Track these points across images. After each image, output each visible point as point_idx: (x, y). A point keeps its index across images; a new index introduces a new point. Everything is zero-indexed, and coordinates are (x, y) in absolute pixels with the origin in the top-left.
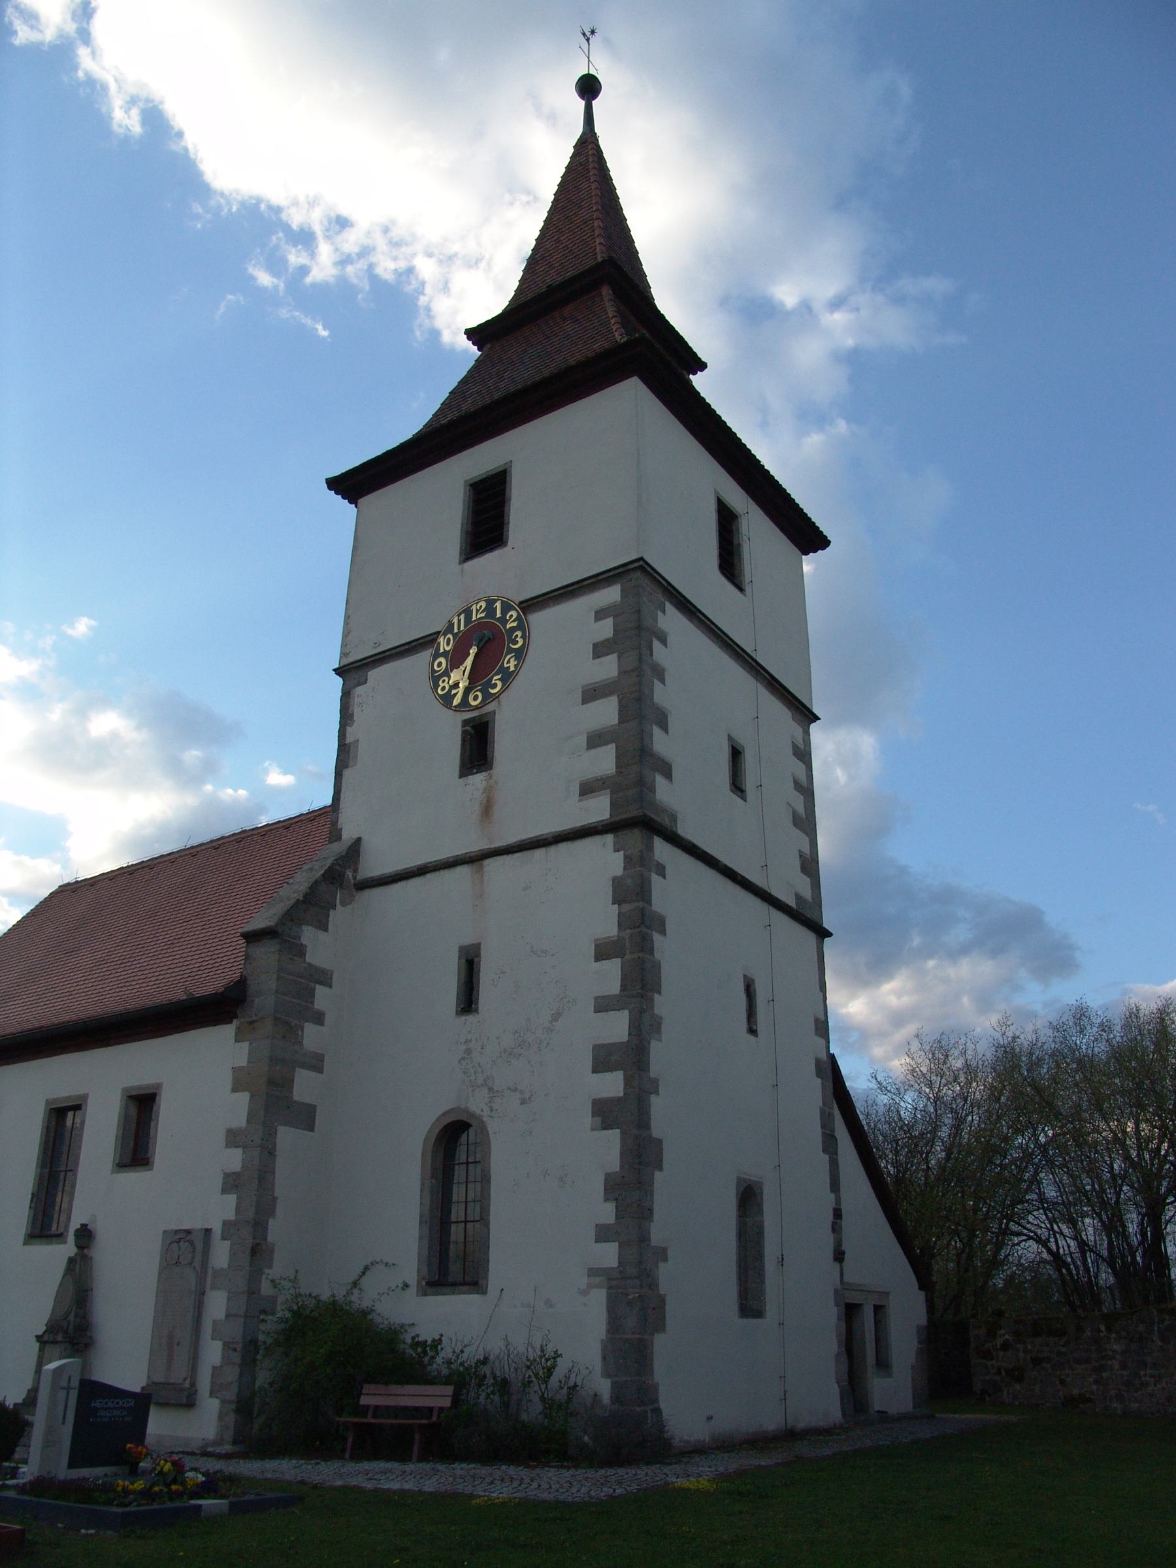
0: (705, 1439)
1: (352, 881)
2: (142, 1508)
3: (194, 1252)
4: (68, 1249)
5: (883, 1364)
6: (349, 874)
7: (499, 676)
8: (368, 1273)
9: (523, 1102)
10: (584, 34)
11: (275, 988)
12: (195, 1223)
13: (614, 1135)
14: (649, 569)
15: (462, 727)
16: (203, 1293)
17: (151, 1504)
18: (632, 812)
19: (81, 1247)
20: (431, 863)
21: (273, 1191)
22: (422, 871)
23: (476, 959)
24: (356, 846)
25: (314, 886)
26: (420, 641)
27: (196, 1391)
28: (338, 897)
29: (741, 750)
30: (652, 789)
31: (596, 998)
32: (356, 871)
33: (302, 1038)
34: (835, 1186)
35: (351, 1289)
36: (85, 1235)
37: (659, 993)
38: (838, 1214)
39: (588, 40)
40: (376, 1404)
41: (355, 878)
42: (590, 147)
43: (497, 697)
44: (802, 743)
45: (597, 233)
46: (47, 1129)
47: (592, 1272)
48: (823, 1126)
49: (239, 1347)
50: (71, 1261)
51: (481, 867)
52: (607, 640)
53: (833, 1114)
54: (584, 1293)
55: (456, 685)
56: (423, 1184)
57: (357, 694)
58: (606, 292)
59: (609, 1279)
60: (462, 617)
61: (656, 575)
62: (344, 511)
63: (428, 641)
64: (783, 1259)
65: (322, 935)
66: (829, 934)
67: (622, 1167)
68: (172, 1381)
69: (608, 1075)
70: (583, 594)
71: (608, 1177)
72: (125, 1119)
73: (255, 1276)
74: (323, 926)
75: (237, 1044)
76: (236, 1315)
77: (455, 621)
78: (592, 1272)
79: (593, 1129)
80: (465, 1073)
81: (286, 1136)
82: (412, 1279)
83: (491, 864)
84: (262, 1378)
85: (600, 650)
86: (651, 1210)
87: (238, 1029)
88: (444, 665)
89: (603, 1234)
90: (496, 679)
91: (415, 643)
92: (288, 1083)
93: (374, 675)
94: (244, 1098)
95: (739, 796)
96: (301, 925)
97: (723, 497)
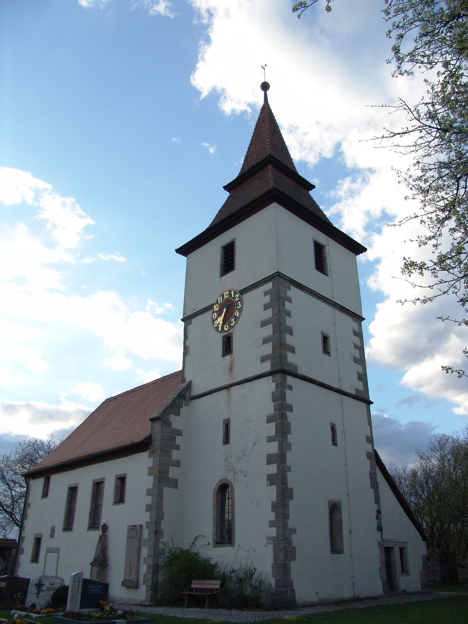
0: (315, 601)
1: (189, 397)
2: (96, 622)
3: (137, 533)
4: (99, 533)
5: (404, 570)
6: (188, 394)
7: (234, 319)
8: (197, 539)
9: (245, 476)
10: (262, 67)
11: (160, 438)
12: (137, 523)
13: (274, 487)
14: (282, 275)
15: (223, 338)
16: (140, 548)
17: (99, 621)
18: (278, 367)
19: (103, 532)
20: (213, 389)
21: (163, 511)
22: (211, 392)
23: (229, 424)
24: (190, 384)
25: (174, 401)
26: (208, 307)
27: (139, 582)
28: (183, 403)
29: (327, 337)
30: (286, 358)
31: (267, 437)
32: (190, 393)
33: (172, 455)
34: (377, 501)
35: (192, 545)
36: (105, 528)
37: (290, 434)
38: (379, 512)
39: (264, 69)
40: (217, 588)
41: (190, 396)
42: (266, 110)
43: (233, 326)
44: (358, 330)
45: (267, 144)
46: (93, 490)
47: (268, 538)
48: (371, 478)
49: (152, 567)
50: (100, 536)
51: (230, 390)
52: (268, 303)
53: (376, 473)
54: (265, 546)
55: (219, 324)
56: (214, 507)
57: (189, 328)
58: (270, 167)
59: (274, 541)
60: (221, 297)
61: (285, 277)
62: (183, 259)
63: (210, 308)
64: (351, 531)
65: (178, 418)
66: (372, 403)
67: (277, 499)
68: (131, 579)
69: (271, 465)
70: (260, 286)
71: (272, 502)
72: (116, 486)
73: (156, 542)
74: (178, 414)
75: (149, 459)
76: (151, 556)
77: (219, 299)
78: (268, 538)
79: (267, 486)
80: (226, 466)
81: (167, 491)
82: (211, 542)
83: (233, 389)
84: (161, 578)
85: (266, 307)
86: (288, 515)
87: (149, 453)
88: (216, 316)
89: (271, 524)
90: (233, 320)
91: (207, 308)
92: (167, 472)
93: (195, 320)
94: (151, 478)
95: (327, 355)
96: (169, 415)
97: (317, 240)
